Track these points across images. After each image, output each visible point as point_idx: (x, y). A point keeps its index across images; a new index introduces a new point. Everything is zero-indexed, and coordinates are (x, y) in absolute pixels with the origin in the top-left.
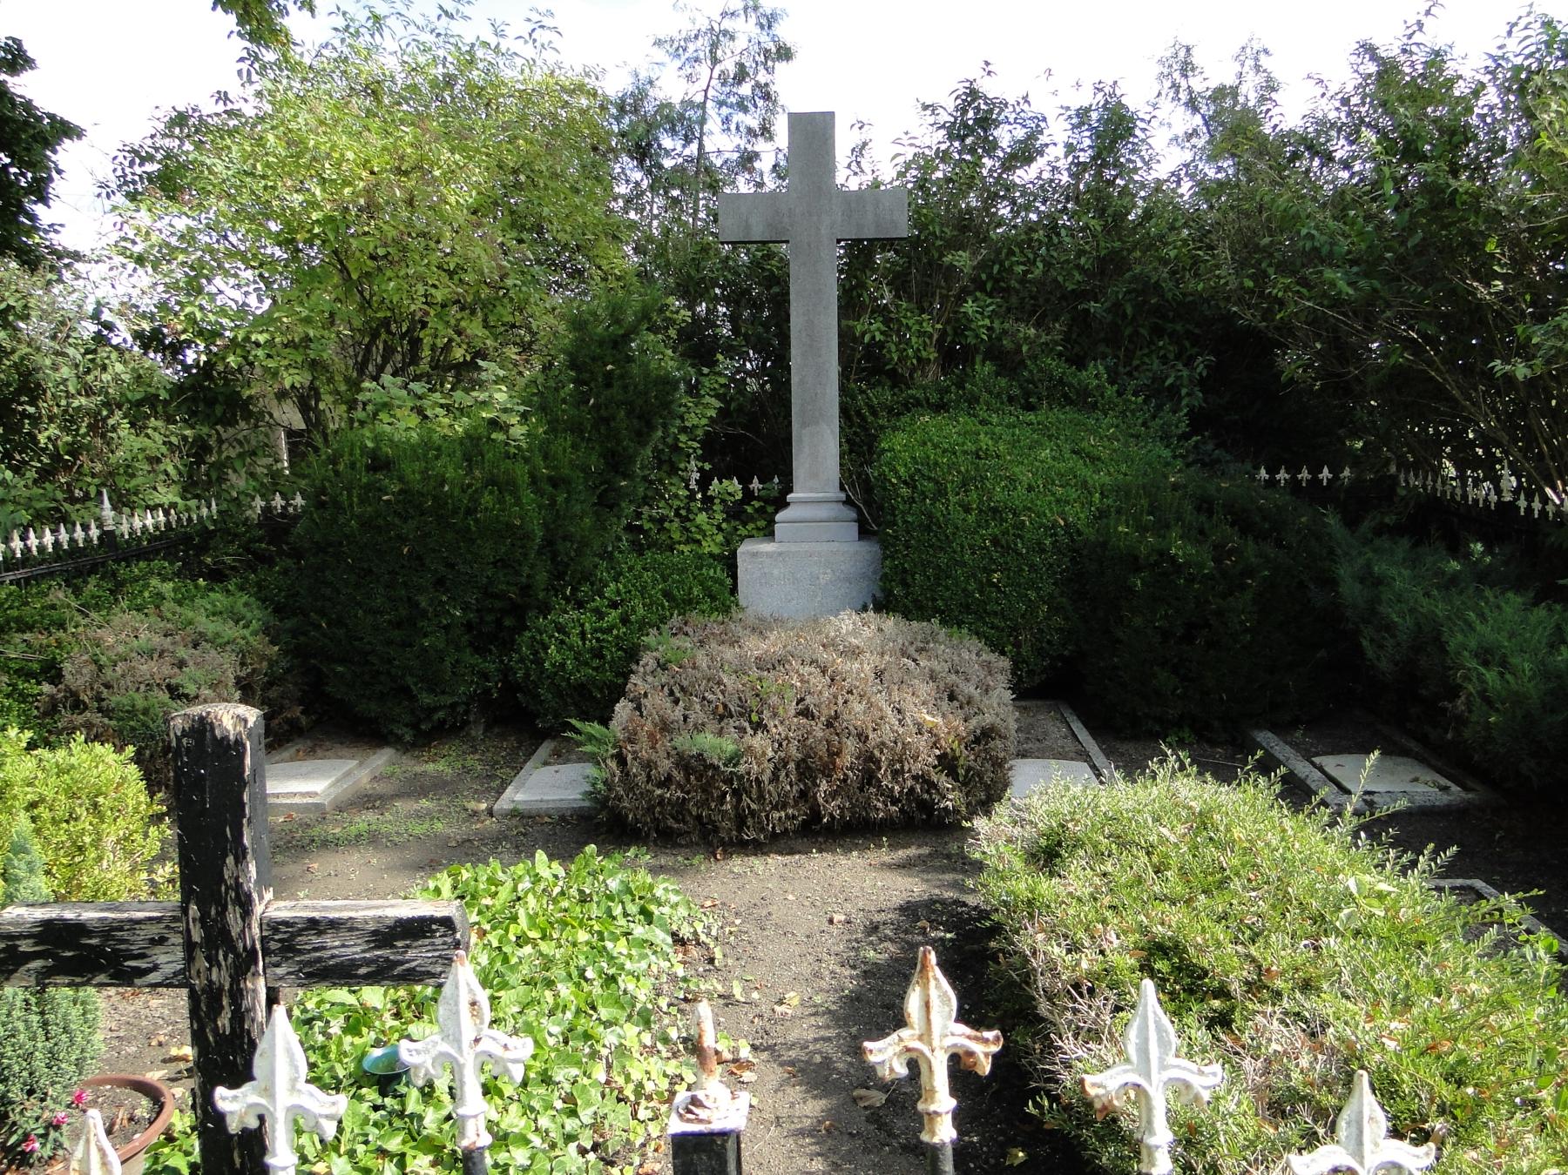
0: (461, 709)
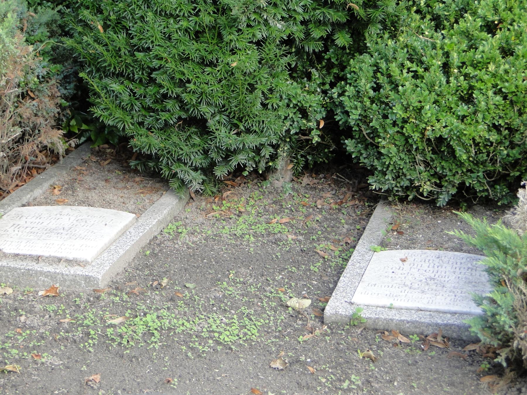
0: (267, 152)
